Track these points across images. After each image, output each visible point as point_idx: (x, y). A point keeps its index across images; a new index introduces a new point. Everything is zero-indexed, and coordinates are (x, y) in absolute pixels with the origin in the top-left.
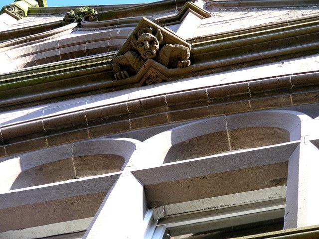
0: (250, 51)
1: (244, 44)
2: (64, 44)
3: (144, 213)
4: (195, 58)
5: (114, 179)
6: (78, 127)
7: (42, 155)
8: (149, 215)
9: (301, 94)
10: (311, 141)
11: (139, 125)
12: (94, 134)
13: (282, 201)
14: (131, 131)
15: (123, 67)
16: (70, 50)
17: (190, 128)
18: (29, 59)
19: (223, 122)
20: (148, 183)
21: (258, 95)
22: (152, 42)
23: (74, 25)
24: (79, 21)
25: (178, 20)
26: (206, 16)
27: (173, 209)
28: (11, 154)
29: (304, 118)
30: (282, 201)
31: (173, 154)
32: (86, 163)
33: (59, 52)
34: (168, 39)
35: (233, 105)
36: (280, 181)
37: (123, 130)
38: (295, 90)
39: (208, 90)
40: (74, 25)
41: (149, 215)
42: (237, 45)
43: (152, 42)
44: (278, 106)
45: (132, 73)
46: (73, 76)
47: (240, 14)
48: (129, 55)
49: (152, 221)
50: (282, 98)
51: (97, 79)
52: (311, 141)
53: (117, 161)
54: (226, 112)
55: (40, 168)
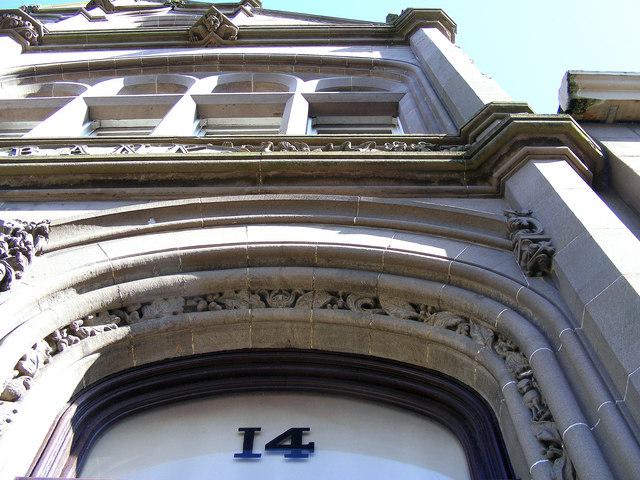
0: (274, 37)
1: (272, 32)
2: (162, 19)
3: (84, 123)
4: (240, 36)
5: (178, 99)
6: (162, 65)
7: (136, 79)
8: (197, 122)
9: (301, 67)
10: (303, 94)
11: (199, 70)
12: (171, 71)
13: (278, 127)
14: (194, 73)
15: (195, 34)
16: (164, 21)
17: (230, 76)
18: (139, 24)
19: (251, 77)
20: (200, 103)
21: (275, 63)
22: (215, 21)
23: (170, 8)
24: (173, 7)
25: (233, 15)
26: (250, 15)
27: (212, 121)
28: (120, 75)
29: (300, 81)
30: (278, 127)
31: (217, 89)
32: (163, 87)
33: (158, 23)
34: (225, 22)
35: (259, 67)
36: (279, 114)
37: (189, 71)
38: (297, 64)
39: (263, 150)
40: (170, 8)
41: (197, 122)
42: (266, 32)
43: (215, 21)
44: (285, 72)
45: (201, 39)
46: (165, 35)
47: (272, 18)
48: (200, 27)
49: (199, 127)
50: (288, 67)
51: (179, 39)
52: (303, 94)
53: (183, 89)
54: (253, 71)
55: (136, 86)
